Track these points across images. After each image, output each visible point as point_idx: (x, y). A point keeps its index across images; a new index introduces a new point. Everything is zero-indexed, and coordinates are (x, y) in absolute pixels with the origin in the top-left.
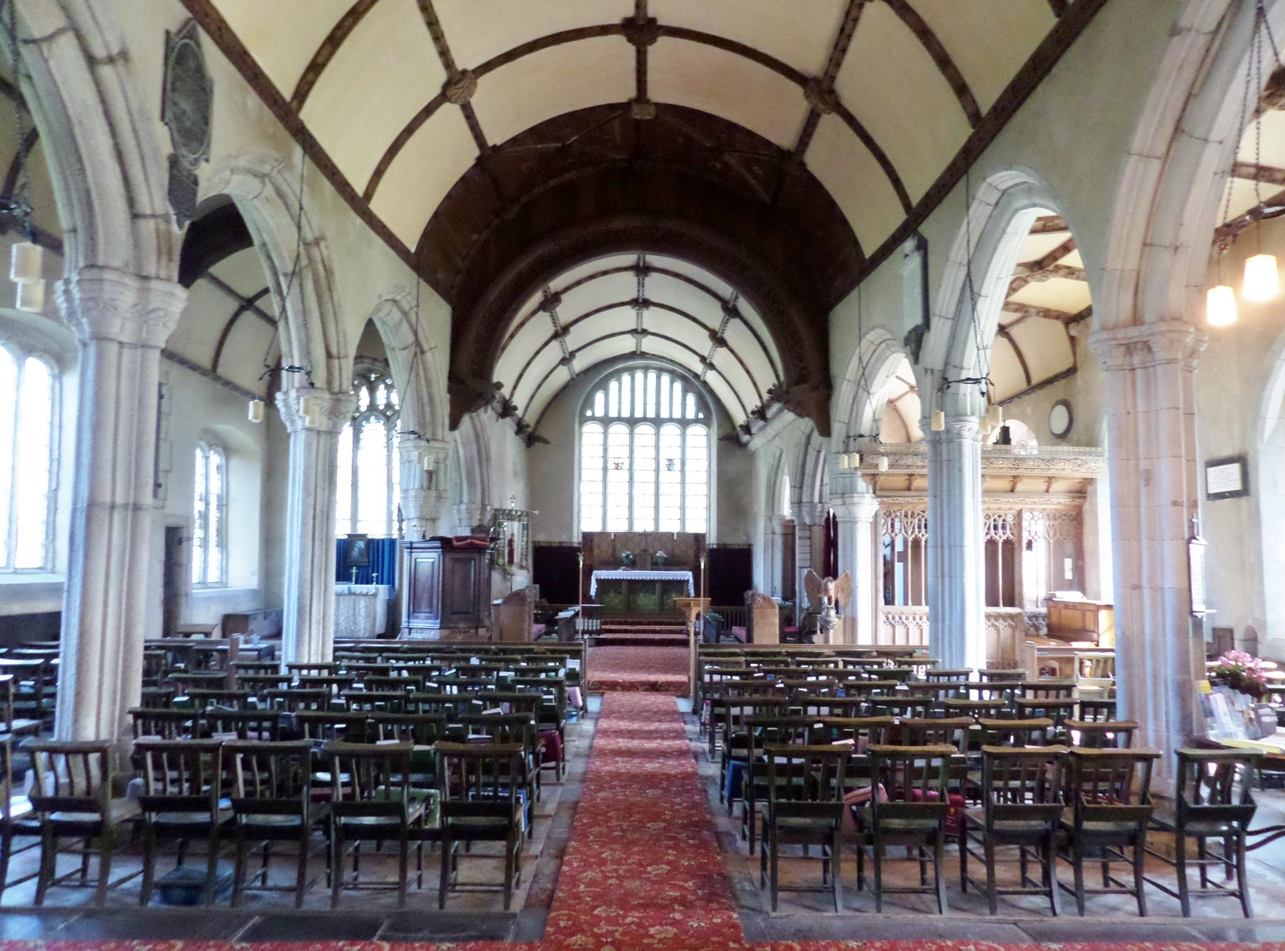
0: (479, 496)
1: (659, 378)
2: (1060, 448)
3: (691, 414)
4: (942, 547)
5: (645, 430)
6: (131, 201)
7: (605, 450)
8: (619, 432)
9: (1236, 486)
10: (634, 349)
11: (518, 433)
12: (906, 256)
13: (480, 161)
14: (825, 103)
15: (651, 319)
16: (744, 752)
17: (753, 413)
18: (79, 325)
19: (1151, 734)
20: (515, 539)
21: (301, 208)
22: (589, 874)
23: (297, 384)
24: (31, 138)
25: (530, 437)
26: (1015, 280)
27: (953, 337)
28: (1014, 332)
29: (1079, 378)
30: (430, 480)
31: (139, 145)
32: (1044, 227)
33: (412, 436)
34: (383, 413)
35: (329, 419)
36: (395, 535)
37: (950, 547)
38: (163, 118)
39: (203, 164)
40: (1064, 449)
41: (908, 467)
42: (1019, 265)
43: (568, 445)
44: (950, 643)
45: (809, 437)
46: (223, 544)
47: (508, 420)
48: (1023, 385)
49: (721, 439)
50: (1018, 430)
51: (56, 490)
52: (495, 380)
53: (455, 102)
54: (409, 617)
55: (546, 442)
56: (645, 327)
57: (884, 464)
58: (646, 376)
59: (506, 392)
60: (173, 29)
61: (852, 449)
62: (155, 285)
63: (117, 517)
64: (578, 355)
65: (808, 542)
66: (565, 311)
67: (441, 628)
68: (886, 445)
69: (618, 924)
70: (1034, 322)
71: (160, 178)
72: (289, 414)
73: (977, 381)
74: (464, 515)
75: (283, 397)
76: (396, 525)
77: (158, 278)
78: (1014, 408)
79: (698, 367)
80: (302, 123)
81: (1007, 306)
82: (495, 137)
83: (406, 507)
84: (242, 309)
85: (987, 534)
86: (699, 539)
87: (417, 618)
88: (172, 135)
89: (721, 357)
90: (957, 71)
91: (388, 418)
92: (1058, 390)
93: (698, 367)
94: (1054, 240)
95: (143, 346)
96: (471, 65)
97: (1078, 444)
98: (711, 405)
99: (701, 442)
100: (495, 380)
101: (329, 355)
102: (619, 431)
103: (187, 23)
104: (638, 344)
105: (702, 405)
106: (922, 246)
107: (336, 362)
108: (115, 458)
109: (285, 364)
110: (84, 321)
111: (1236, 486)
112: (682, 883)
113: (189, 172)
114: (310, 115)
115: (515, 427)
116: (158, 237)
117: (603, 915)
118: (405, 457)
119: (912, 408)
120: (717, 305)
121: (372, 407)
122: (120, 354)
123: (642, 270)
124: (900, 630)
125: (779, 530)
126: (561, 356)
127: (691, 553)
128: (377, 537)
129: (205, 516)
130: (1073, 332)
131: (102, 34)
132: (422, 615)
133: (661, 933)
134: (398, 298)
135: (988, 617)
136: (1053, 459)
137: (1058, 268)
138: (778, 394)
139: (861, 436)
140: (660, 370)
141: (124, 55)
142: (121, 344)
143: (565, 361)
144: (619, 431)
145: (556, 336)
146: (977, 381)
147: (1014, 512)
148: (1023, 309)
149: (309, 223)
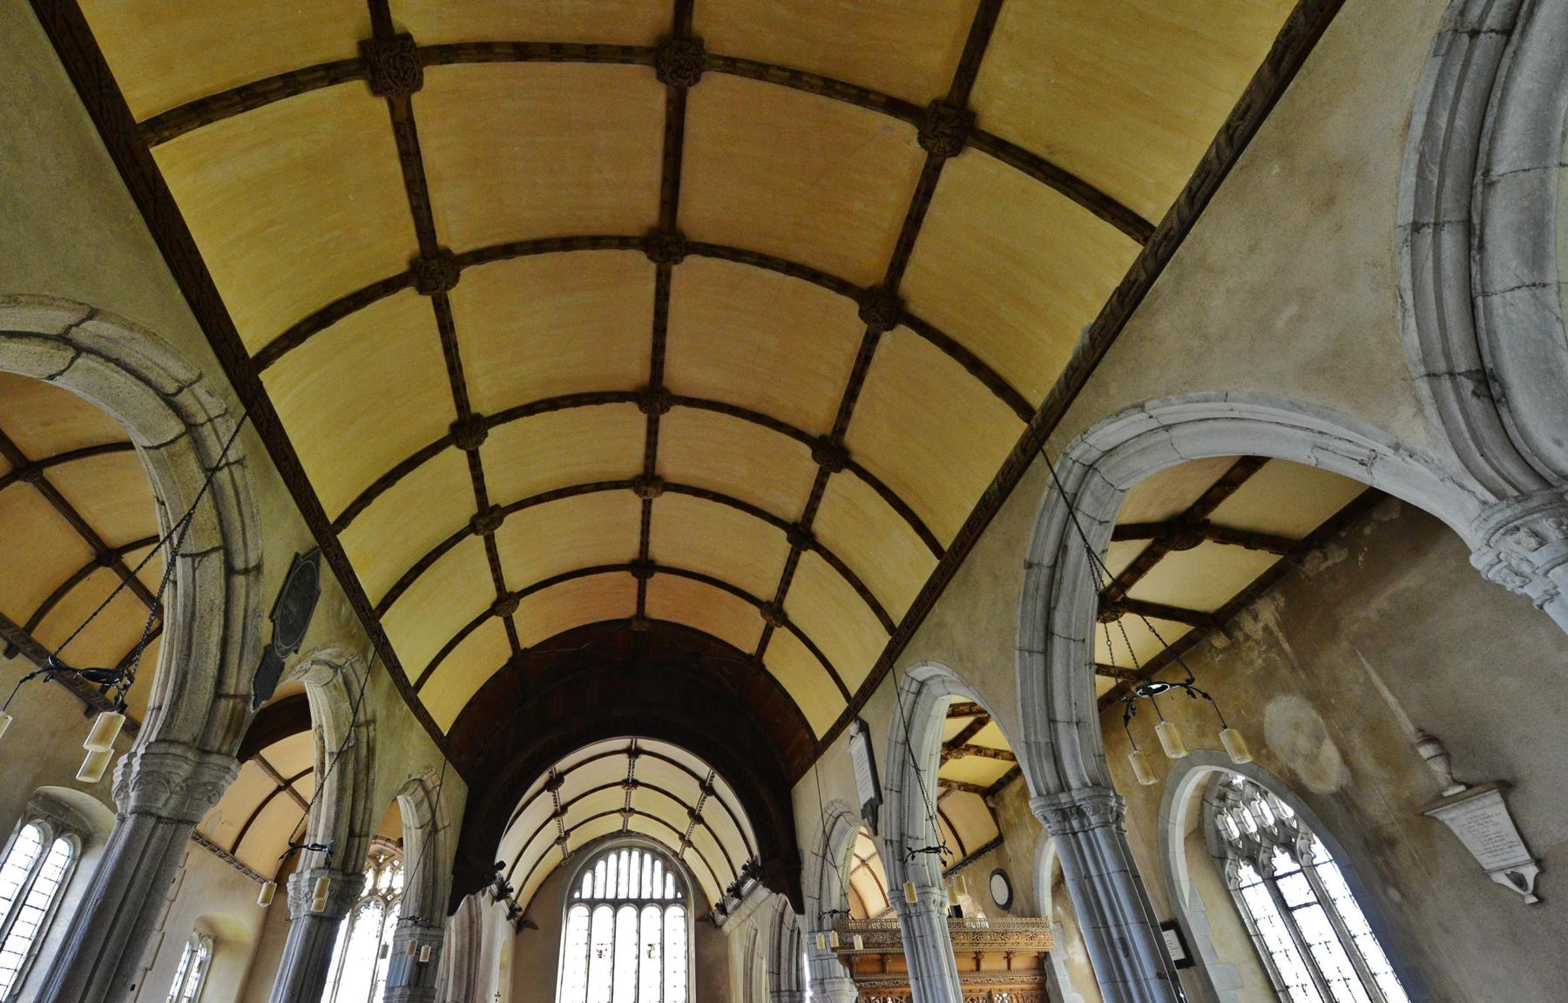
1: (642, 856)
3: (670, 894)
5: (628, 912)
6: (220, 681)
10: (621, 828)
11: (509, 918)
12: (852, 737)
13: (511, 661)
14: (776, 618)
15: (639, 798)
21: (362, 694)
23: (313, 865)
24: (160, 630)
25: (521, 922)
27: (901, 808)
29: (1007, 846)
31: (244, 637)
33: (410, 922)
34: (384, 897)
35: (336, 903)
39: (293, 655)
41: (879, 945)
47: (503, 902)
49: (697, 920)
55: (535, 927)
56: (632, 806)
57: (858, 942)
58: (630, 855)
60: (302, 553)
62: (216, 760)
66: (566, 792)
70: (958, 795)
71: (251, 662)
72: (296, 898)
73: (937, 850)
75: (295, 879)
77: (219, 752)
79: (676, 845)
84: (279, 789)
88: (274, 630)
89: (698, 834)
91: (387, 903)
93: (676, 845)
96: (517, 589)
97: (1023, 915)
98: (688, 888)
101: (352, 834)
102: (604, 912)
103: (316, 548)
104: (625, 823)
105: (680, 885)
106: (864, 728)
107: (357, 840)
108: (102, 952)
109: (307, 841)
113: (278, 660)
114: (389, 622)
115: (508, 911)
116: (232, 715)
118: (399, 948)
121: (374, 891)
130: (992, 805)
134: (425, 778)
137: (968, 748)
138: (751, 870)
139: (835, 912)
140: (643, 850)
141: (258, 568)
142: (159, 818)
143: (560, 840)
144: (604, 912)
146: (937, 850)
147: (984, 994)
149: (365, 710)
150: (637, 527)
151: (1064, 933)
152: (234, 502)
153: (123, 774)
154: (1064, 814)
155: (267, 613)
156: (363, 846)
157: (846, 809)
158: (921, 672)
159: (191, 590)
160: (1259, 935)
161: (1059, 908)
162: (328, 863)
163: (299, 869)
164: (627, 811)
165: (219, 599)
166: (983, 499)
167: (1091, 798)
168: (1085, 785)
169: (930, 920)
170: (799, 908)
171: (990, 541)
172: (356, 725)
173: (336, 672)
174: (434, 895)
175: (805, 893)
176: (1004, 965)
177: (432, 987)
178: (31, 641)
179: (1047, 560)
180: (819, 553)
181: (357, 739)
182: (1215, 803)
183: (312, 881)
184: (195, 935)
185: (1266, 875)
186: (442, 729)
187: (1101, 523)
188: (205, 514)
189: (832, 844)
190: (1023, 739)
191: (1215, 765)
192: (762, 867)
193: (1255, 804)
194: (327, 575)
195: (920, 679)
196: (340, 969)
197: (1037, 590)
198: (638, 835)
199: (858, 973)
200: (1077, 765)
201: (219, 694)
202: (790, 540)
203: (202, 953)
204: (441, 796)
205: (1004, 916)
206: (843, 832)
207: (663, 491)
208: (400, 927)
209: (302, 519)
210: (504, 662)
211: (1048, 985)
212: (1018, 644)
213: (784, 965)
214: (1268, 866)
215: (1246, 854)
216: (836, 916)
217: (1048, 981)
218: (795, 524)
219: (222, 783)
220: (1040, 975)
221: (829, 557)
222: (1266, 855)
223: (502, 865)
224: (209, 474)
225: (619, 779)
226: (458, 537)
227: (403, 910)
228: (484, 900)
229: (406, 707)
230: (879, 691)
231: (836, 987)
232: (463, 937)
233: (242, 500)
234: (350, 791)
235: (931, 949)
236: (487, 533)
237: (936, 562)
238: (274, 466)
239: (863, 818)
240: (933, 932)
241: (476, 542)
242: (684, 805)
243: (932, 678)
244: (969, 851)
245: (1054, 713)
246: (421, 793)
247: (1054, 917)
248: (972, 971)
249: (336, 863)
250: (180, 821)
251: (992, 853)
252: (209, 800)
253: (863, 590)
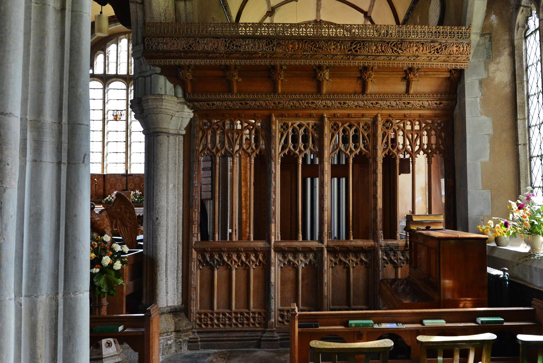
85: (283, 148)
147: (369, 120)
151: (491, 47)
161: (493, 17)
211: (457, 111)
217: (457, 107)
220: (447, 100)
247: (484, 28)
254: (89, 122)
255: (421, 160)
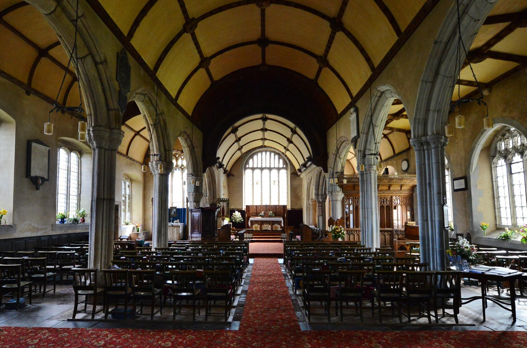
0: (212, 194)
1: (270, 154)
2: (404, 175)
3: (281, 165)
4: (365, 209)
5: (266, 172)
6: (107, 105)
7: (253, 178)
8: (257, 172)
9: (463, 186)
11: (224, 173)
12: (351, 113)
13: (211, 86)
15: (267, 135)
16: (301, 274)
17: (302, 165)
18: (92, 143)
19: (432, 267)
20: (225, 208)
21: (157, 104)
22: (252, 311)
25: (229, 174)
26: (389, 119)
28: (390, 137)
30: (197, 189)
32: (397, 102)
34: (181, 167)
36: (186, 207)
37: (367, 209)
38: (116, 80)
40: (407, 175)
41: (353, 182)
42: (389, 115)
43: (240, 177)
44: (368, 240)
45: (321, 173)
46: (131, 210)
47: (221, 169)
48: (392, 154)
49: (291, 174)
50: (391, 169)
51: (80, 194)
52: (217, 156)
53: (203, 68)
54: (191, 233)
55: (233, 176)
56: (265, 137)
57: (345, 181)
58: (266, 153)
59: (220, 160)
61: (335, 177)
62: (115, 131)
63: (105, 202)
64: (243, 147)
65: (321, 208)
66: (239, 133)
67: (201, 237)
68: (346, 175)
69: (262, 325)
72: (153, 169)
73: (375, 154)
74: (208, 200)
76: (186, 204)
77: (116, 129)
78: (390, 162)
79: (283, 150)
80: (157, 77)
81: (386, 128)
82: (216, 78)
83: (189, 197)
85: (380, 204)
86: (284, 207)
87: (194, 233)
89: (291, 147)
90: (367, 54)
91: (182, 169)
92: (404, 156)
94: (399, 107)
95: (111, 150)
96: (209, 56)
97: (411, 174)
98: (288, 163)
99: (284, 175)
100: (217, 156)
101: (165, 150)
103: (123, 49)
104: (263, 143)
105: (285, 163)
106: (357, 111)
110: (94, 142)
111: (463, 186)
112: (285, 333)
115: (223, 171)
117: (256, 346)
119: (355, 162)
120: (289, 130)
121: (177, 166)
122: (105, 152)
123: (264, 119)
124: (352, 236)
125: (311, 203)
126: (238, 148)
127: (282, 211)
128: (179, 208)
129: (125, 202)
131: (99, 55)
132: (195, 233)
133: (275, 327)
134: (186, 131)
135: (381, 231)
136: (402, 179)
138: (309, 159)
139: (338, 172)
141: (105, 61)
142: (105, 149)
143: (240, 149)
144: (257, 172)
145: (236, 141)
147: (390, 196)
148: (392, 129)
150: (259, 22)
152: (87, 34)
153: (88, 136)
154: (422, 144)
155: (115, 79)
156: (170, 154)
157: (346, 139)
158: (383, 88)
159: (85, 72)
160: (497, 182)
162: (160, 160)
163: (151, 161)
164: (264, 139)
165: (96, 75)
166: (424, 7)
167: (433, 139)
168: (433, 134)
169: (370, 175)
170: (326, 171)
171: (422, 29)
172: (157, 115)
173: (145, 97)
174: (197, 167)
175: (329, 166)
176: (399, 188)
177: (202, 192)
178: (32, 89)
179: (445, 39)
180: (344, 33)
181: (159, 120)
182: (500, 137)
183: (157, 165)
184: (124, 178)
185: (508, 162)
186: (189, 114)
187: (475, 20)
188: (80, 42)
189: (340, 151)
190: (414, 117)
191: (504, 123)
192: (313, 158)
193: (516, 138)
194: (131, 60)
195: (382, 90)
196: (172, 187)
197: (436, 54)
198: (269, 147)
199: (345, 190)
200: (433, 127)
201: (109, 110)
202: (331, 27)
203: (128, 183)
204: (193, 137)
205: (404, 174)
206: (344, 147)
207: (270, 3)
208: (188, 177)
209: (114, 36)
210: (208, 86)
212: (421, 79)
213: (320, 187)
214: (511, 159)
215: (504, 155)
216: (338, 174)
218: (334, 18)
219: (120, 138)
221: (349, 35)
222: (512, 156)
223: (219, 158)
224: (75, 23)
225: (260, 128)
226: (179, 35)
227: (188, 172)
228: (215, 168)
229: (174, 107)
230: (364, 95)
231: (336, 194)
232: (209, 179)
233: (90, 33)
234: (161, 137)
235: (369, 184)
236: (192, 31)
237: (396, 38)
238: (96, 15)
239: (352, 142)
240: (371, 179)
241: (187, 36)
242: (285, 137)
243: (387, 90)
244: (397, 152)
245: (430, 106)
246: (186, 136)
248: (387, 190)
249: (163, 159)
250: (111, 150)
251: (405, 154)
252: (118, 143)
253: (362, 51)
254: (281, 206)
255: (399, 207)
